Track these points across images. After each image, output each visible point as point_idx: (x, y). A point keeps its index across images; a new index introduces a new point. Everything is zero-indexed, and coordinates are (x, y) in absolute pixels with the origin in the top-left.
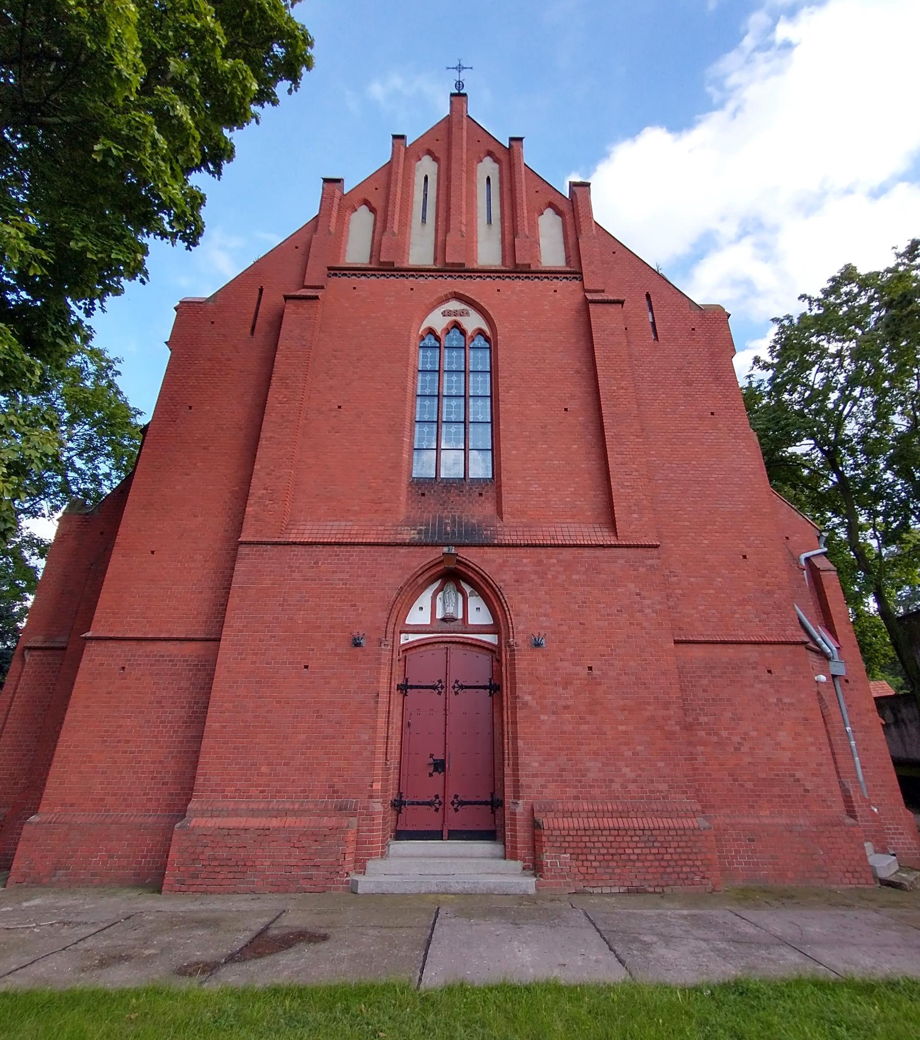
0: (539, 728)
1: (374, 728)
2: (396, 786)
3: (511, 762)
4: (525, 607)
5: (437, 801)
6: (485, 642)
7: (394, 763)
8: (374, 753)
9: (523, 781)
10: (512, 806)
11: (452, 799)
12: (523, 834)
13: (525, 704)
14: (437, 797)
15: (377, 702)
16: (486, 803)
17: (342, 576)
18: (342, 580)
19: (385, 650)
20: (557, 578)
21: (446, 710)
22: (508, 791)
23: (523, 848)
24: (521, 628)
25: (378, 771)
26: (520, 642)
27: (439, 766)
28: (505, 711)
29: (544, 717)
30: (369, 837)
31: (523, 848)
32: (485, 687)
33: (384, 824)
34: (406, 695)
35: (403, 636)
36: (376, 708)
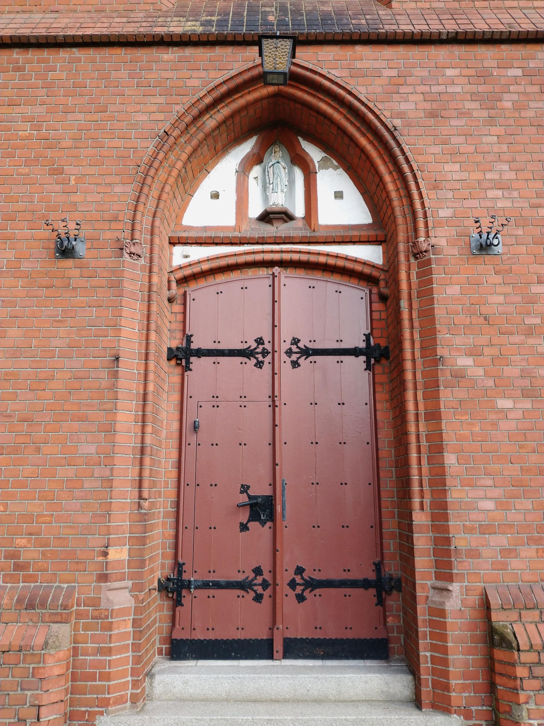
0: (494, 425)
1: (109, 430)
2: (170, 551)
3: (427, 501)
4: (452, 170)
5: (259, 580)
6: (356, 261)
7: (162, 505)
8: (108, 482)
9: (460, 540)
10: (436, 598)
11: (290, 575)
12: (462, 657)
13: (459, 376)
14: (258, 571)
15: (115, 375)
16: (365, 584)
17: (29, 110)
18: (30, 120)
19: (133, 272)
20: (526, 108)
21: (274, 406)
22: (423, 563)
23: (464, 688)
24: (444, 213)
25: (122, 521)
26: (443, 242)
27: (262, 509)
28: (410, 395)
29: (504, 403)
30: (101, 664)
31: (464, 688)
32: (354, 352)
33: (138, 634)
34: (187, 368)
35: (178, 250)
36: (113, 387)
